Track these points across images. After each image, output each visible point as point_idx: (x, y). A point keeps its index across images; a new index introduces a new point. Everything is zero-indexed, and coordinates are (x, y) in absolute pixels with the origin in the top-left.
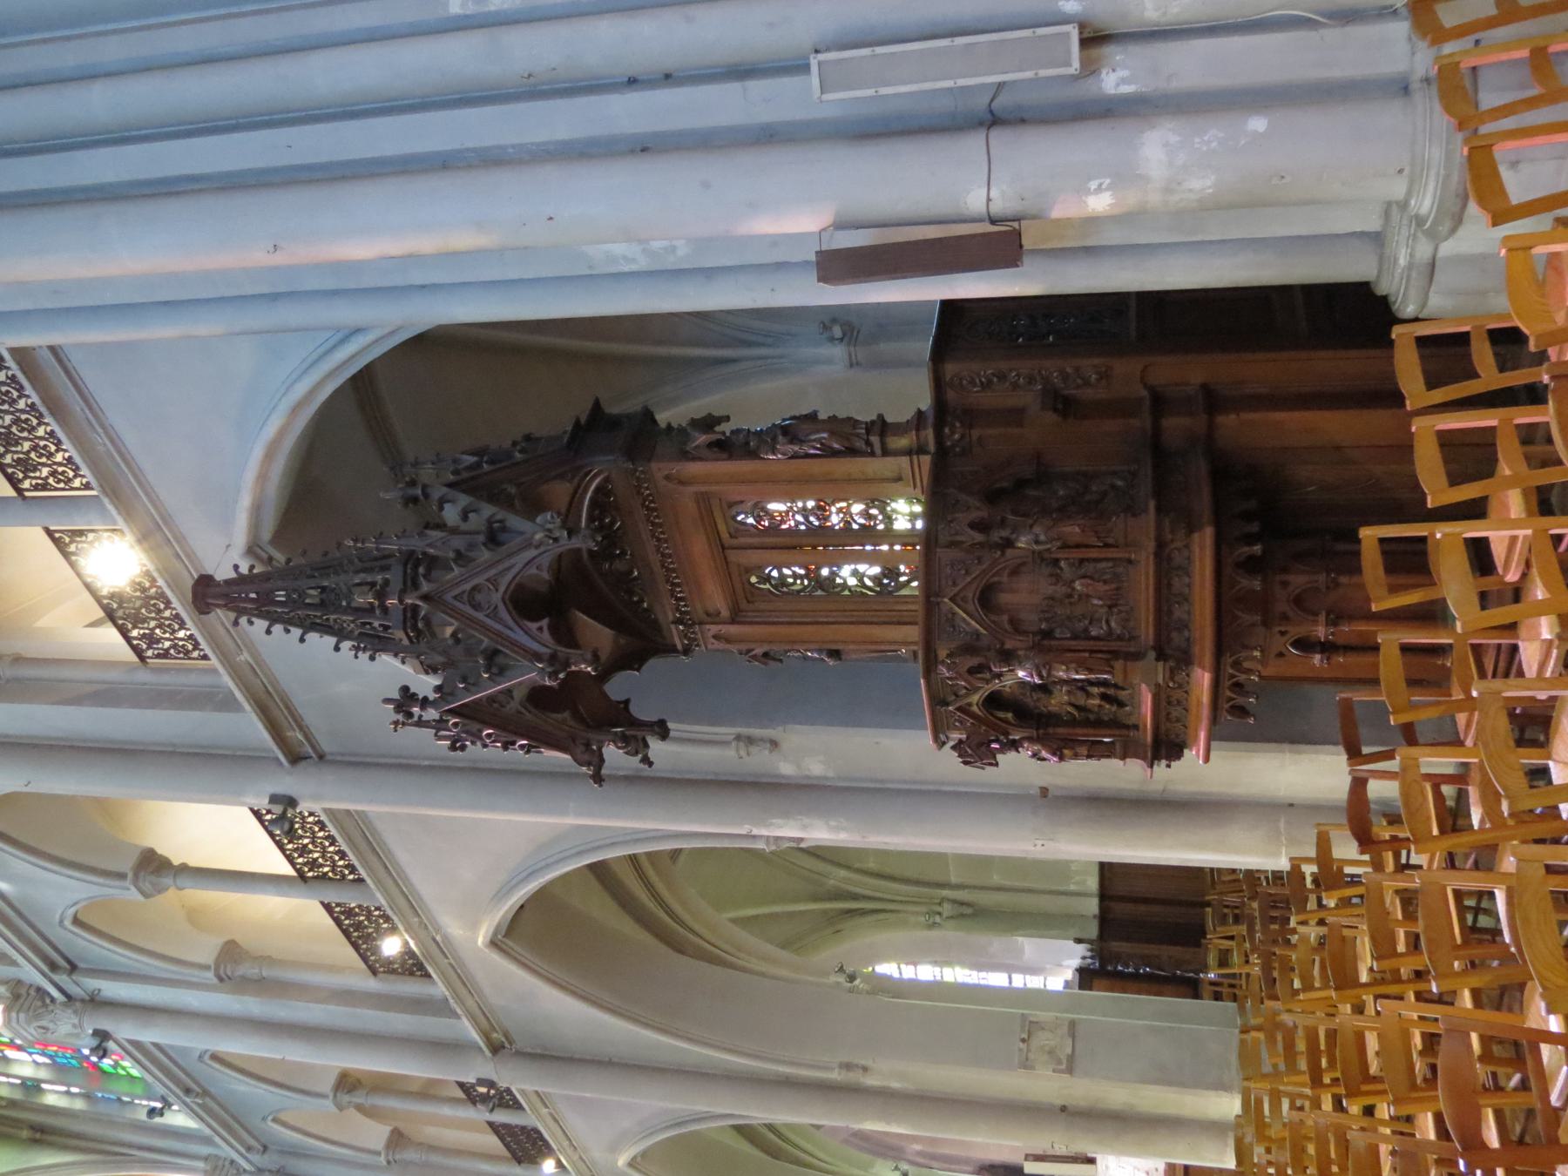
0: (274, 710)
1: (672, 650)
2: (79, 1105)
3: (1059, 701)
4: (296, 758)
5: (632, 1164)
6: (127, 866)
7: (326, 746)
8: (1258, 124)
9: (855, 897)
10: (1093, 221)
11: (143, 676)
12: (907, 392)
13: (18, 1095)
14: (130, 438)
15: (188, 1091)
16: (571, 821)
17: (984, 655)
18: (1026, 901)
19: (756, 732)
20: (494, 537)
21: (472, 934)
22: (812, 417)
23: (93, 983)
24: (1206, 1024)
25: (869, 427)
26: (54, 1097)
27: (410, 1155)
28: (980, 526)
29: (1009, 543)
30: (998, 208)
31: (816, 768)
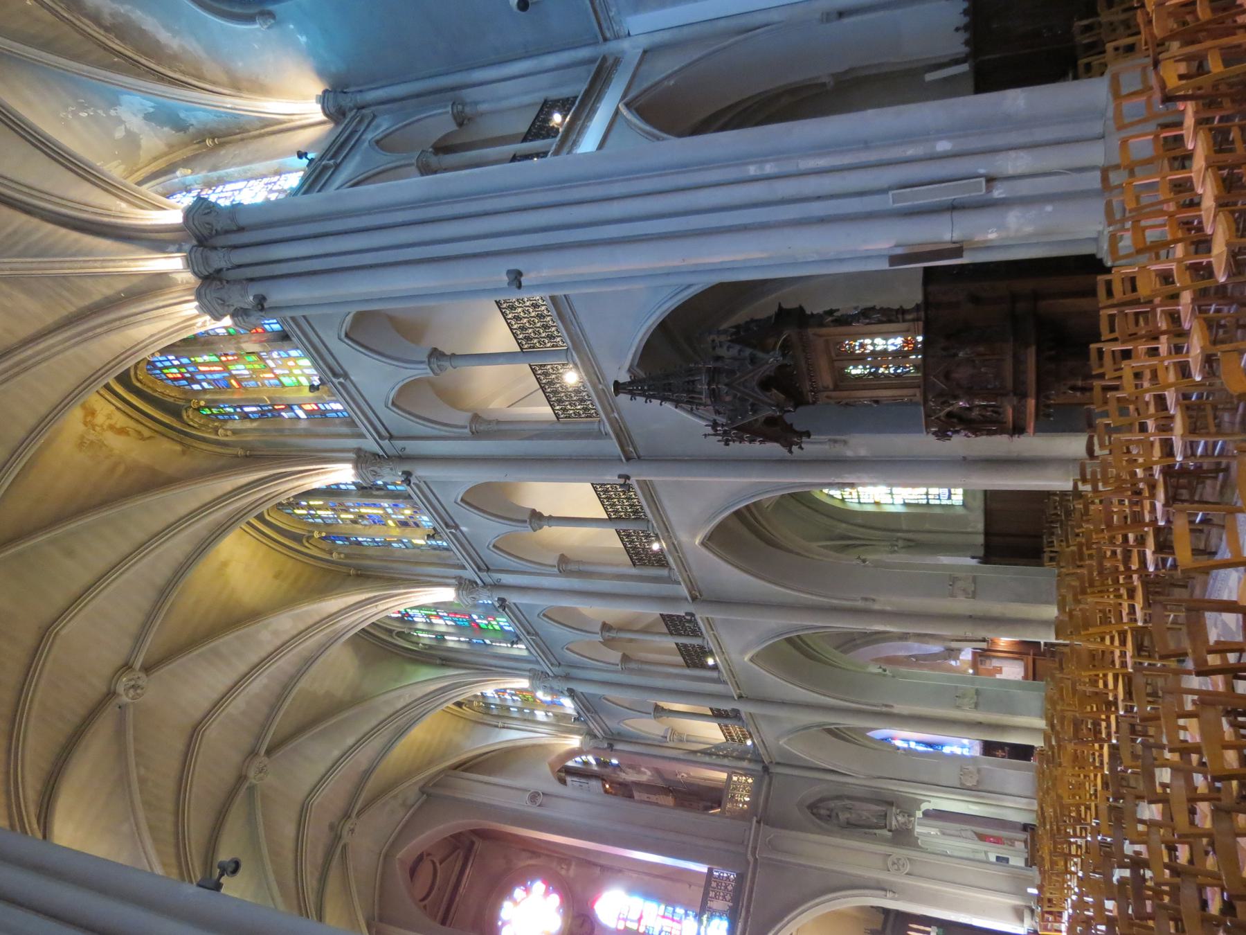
0: (623, 436)
1: (808, 403)
2: (465, 646)
3: (975, 414)
4: (628, 459)
5: (751, 660)
6: (526, 517)
7: (642, 453)
8: (1049, 208)
9: (850, 538)
10: (991, 240)
11: (559, 426)
12: (913, 295)
13: (434, 643)
14: (587, 330)
15: (529, 633)
16: (754, 480)
17: (946, 397)
18: (944, 538)
19: (838, 437)
20: (753, 360)
21: (693, 540)
22: (873, 309)
23: (497, 576)
24: (1043, 576)
25: (897, 311)
26: (452, 641)
27: (633, 665)
28: (944, 349)
29: (956, 355)
30: (955, 239)
31: (863, 452)
